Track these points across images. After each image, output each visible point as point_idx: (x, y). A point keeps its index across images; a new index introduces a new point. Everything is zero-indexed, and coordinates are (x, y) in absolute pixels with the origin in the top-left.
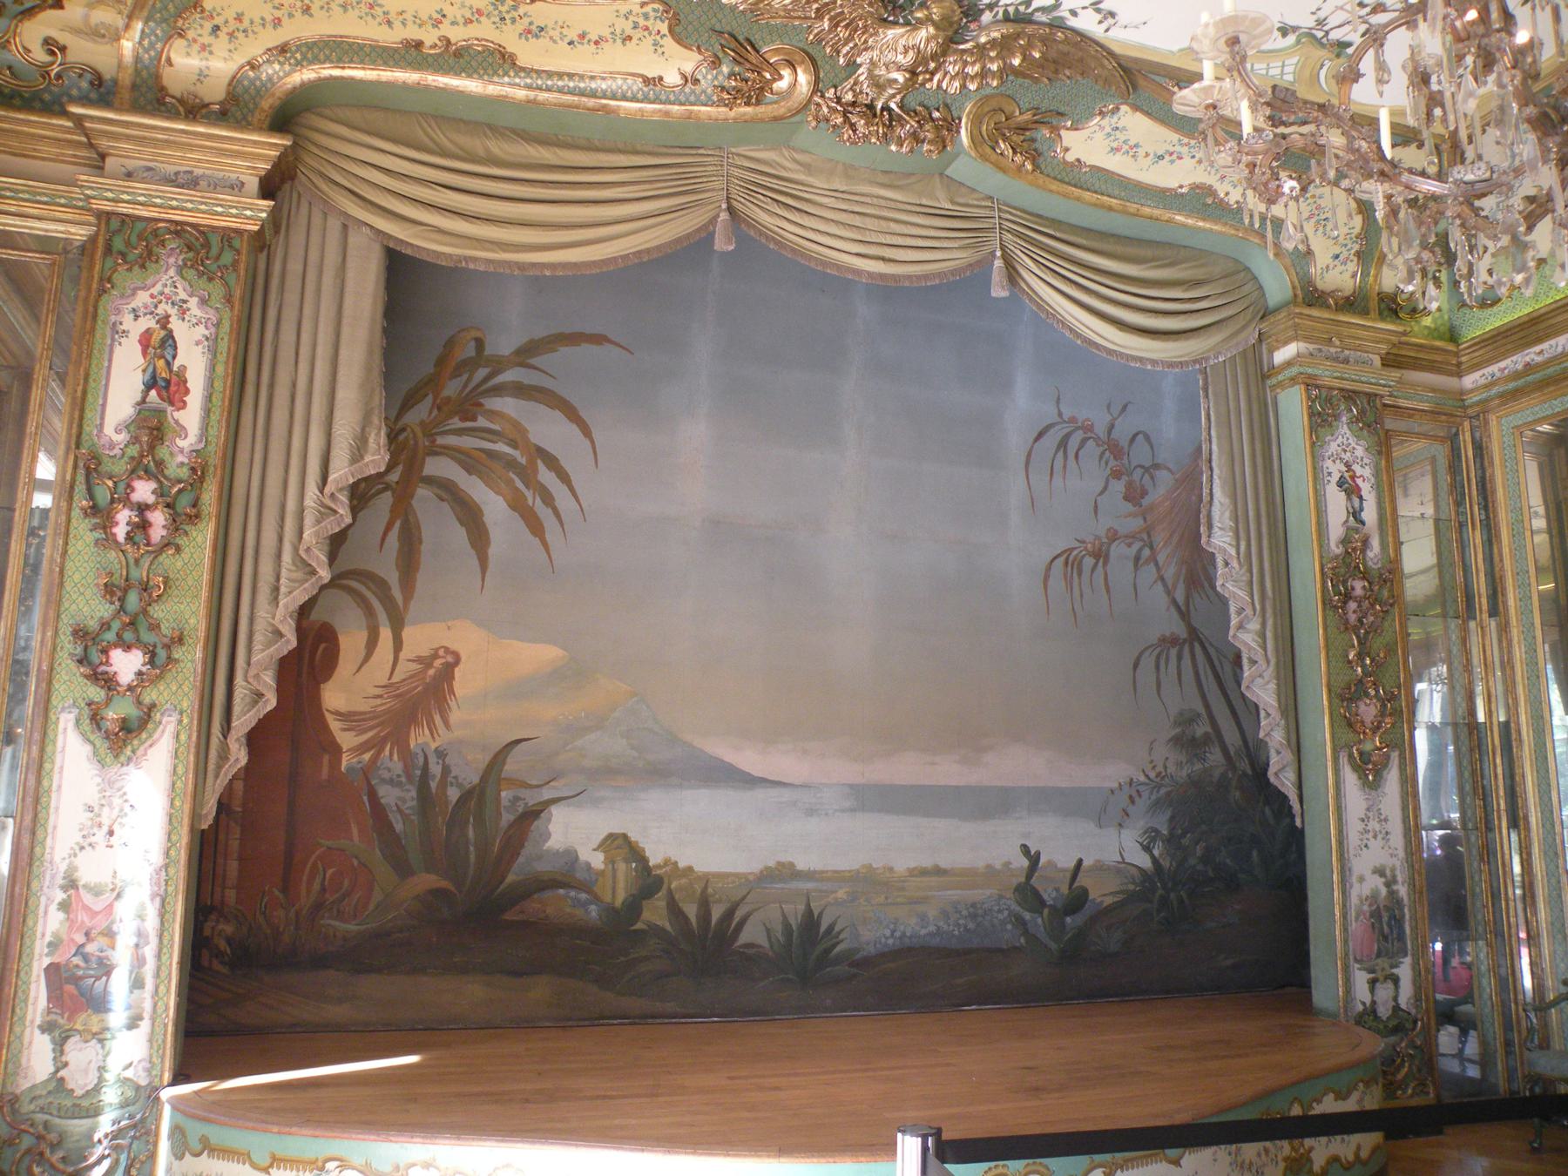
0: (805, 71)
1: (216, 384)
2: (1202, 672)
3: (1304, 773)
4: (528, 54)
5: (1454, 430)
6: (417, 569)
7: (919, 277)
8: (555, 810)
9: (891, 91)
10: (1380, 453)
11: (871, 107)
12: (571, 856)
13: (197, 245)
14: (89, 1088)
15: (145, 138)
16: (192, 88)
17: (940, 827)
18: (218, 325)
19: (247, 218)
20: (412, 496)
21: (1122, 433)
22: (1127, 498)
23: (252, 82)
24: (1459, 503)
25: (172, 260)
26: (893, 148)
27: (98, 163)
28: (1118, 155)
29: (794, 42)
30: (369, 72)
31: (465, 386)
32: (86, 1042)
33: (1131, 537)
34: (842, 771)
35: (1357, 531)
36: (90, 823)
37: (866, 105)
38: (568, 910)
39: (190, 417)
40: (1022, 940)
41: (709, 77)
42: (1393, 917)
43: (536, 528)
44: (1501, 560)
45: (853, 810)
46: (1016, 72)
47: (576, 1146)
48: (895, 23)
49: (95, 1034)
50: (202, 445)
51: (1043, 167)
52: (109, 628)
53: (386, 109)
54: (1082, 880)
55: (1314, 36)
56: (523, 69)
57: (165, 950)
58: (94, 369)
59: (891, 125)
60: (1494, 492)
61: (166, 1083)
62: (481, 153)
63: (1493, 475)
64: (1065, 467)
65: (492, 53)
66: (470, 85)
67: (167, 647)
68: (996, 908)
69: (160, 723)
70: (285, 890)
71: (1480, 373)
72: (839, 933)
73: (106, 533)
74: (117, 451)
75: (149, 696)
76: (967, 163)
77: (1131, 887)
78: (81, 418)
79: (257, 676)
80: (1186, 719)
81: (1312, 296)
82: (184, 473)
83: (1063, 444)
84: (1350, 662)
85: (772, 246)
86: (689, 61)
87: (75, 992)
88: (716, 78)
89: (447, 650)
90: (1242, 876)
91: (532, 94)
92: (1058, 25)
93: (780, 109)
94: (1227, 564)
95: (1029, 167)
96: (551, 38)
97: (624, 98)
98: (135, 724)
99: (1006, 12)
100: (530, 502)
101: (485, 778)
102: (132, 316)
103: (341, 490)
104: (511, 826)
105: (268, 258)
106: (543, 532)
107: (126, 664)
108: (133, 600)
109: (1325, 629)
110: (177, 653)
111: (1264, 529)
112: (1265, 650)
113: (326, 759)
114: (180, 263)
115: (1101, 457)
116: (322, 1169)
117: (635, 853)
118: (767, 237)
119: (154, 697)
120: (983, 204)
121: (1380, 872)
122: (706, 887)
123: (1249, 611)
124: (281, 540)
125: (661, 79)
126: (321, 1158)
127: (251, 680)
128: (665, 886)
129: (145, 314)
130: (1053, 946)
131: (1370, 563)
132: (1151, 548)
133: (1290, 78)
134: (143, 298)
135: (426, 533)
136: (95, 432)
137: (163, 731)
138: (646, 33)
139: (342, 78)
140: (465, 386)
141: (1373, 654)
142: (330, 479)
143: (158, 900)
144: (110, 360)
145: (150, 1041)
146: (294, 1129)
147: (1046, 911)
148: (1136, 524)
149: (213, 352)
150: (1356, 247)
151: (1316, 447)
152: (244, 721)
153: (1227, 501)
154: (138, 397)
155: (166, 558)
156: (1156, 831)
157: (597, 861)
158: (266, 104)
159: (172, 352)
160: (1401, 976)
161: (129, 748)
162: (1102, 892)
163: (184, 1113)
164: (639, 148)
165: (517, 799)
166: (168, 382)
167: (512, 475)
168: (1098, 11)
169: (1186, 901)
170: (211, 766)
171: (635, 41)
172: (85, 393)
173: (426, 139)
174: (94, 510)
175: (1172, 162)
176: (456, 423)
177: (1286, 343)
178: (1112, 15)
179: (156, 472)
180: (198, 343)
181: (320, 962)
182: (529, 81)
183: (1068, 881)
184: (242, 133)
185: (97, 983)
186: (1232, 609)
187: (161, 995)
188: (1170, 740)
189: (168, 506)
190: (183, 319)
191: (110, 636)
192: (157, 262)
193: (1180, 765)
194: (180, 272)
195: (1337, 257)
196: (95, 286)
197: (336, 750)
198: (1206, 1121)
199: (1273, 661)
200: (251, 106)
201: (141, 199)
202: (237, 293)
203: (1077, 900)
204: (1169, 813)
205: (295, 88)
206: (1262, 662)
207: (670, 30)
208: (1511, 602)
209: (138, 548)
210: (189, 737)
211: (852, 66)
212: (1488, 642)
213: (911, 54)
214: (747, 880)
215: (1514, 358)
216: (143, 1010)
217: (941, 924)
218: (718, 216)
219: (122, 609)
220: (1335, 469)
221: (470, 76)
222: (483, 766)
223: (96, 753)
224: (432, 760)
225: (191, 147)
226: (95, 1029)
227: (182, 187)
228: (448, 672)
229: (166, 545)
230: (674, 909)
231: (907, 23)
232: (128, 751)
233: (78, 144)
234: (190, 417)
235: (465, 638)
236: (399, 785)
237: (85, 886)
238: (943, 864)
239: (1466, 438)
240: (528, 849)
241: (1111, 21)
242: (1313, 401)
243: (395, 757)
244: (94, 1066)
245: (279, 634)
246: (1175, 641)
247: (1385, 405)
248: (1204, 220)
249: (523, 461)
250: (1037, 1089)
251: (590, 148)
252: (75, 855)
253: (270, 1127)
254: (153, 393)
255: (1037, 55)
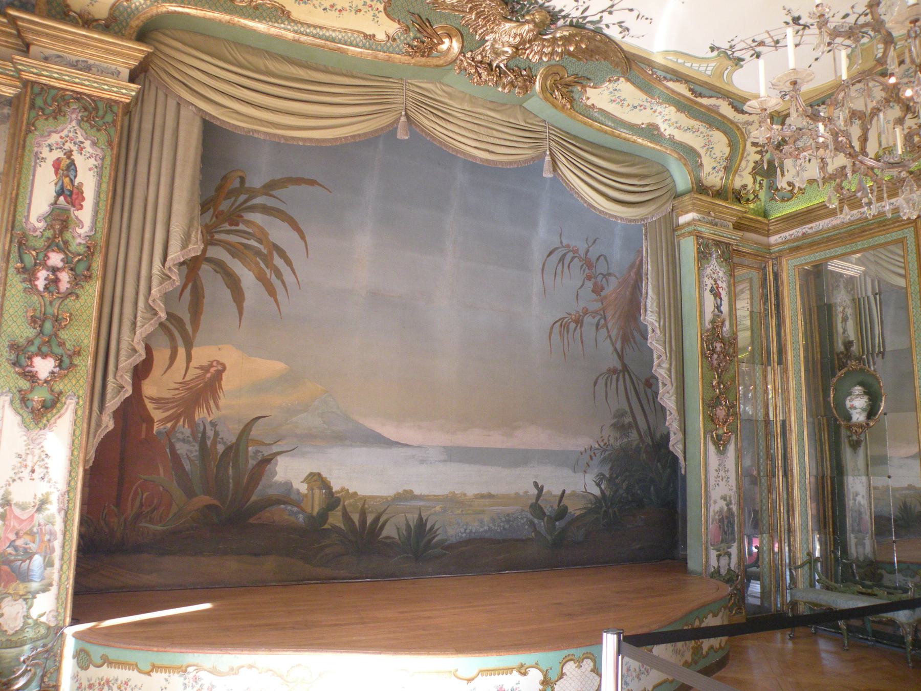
0: (457, 41)
1: (102, 196)
2: (628, 388)
3: (687, 447)
4: (298, 12)
5: (763, 265)
6: (201, 313)
7: (507, 163)
8: (280, 459)
9: (503, 58)
10: (731, 275)
11: (490, 65)
12: (288, 486)
13: (90, 107)
14: (17, 629)
15: (58, 37)
16: (87, 8)
17: (492, 471)
18: (103, 159)
19: (123, 94)
20: (199, 269)
21: (592, 255)
22: (593, 291)
23: (125, 9)
24: (765, 303)
25: (74, 116)
26: (500, 89)
27: (26, 49)
28: (614, 103)
29: (453, 24)
30: (199, 12)
31: (233, 204)
32: (16, 600)
33: (595, 313)
34: (441, 439)
35: (718, 316)
36: (19, 465)
37: (488, 64)
38: (287, 517)
39: (85, 215)
40: (533, 534)
41: (402, 38)
42: (729, 522)
43: (272, 292)
44: (785, 335)
45: (445, 461)
46: (570, 54)
47: (341, 652)
48: (511, 20)
49: (21, 596)
50: (93, 233)
51: (575, 107)
52: (33, 344)
53: (202, 34)
54: (565, 502)
55: (727, 53)
56: (294, 21)
57: (67, 543)
58: (23, 181)
59: (500, 76)
60: (783, 299)
61: (67, 624)
62: (263, 68)
63: (783, 290)
64: (562, 272)
65: (276, 9)
66: (261, 27)
67: (70, 357)
68: (520, 517)
69: (65, 403)
70: (118, 504)
71: (779, 236)
72: (437, 530)
73: (31, 284)
74: (38, 233)
75: (58, 386)
76: (536, 103)
77: (590, 506)
78: (15, 211)
79: (122, 376)
80: (620, 414)
81: (701, 188)
82: (82, 249)
83: (562, 259)
84: (713, 386)
85: (428, 139)
86: (393, 28)
87: (9, 570)
88: (406, 39)
89: (218, 362)
90: (645, 500)
91: (297, 36)
92: (598, 32)
93: (434, 61)
94: (653, 331)
95: (569, 106)
96: (314, 5)
97: (351, 45)
98: (49, 404)
99: (572, 21)
100: (268, 276)
101: (239, 439)
102: (48, 149)
103: (174, 265)
104: (254, 468)
105: (130, 121)
106: (276, 295)
107: (44, 367)
108: (48, 326)
109: (702, 368)
110: (77, 361)
111: (672, 313)
112: (670, 377)
113: (144, 426)
114: (79, 118)
115: (581, 268)
116: (185, 671)
117: (325, 485)
118: (426, 133)
119: (61, 388)
120: (541, 124)
121: (724, 498)
122: (364, 504)
123: (664, 357)
124: (137, 293)
125: (374, 36)
126: (185, 664)
127: (117, 378)
128: (342, 503)
129: (57, 148)
130: (549, 537)
131: (724, 334)
132: (605, 320)
133: (709, 73)
134: (55, 138)
135: (207, 292)
136: (24, 220)
137: (67, 409)
138: (370, 9)
139: (182, 13)
140: (233, 204)
141: (724, 383)
142: (168, 258)
143: (63, 513)
144: (34, 176)
145: (57, 599)
146: (168, 649)
147: (546, 519)
148: (597, 306)
149: (100, 176)
150: (725, 164)
151: (700, 269)
152: (113, 403)
153: (655, 297)
154: (52, 200)
155: (70, 301)
156: (604, 475)
157: (303, 488)
158: (135, 23)
159: (74, 174)
160: (732, 553)
161: (45, 418)
162: (575, 508)
163: (83, 640)
164: (354, 73)
165: (257, 452)
166: (71, 192)
167: (258, 259)
168: (621, 27)
169: (617, 514)
170: (92, 430)
171: (362, 12)
172: (17, 195)
173: (228, 54)
174: (24, 270)
175: (640, 110)
176: (227, 226)
177: (687, 212)
178: (628, 30)
179: (64, 248)
180: (90, 169)
181: (139, 549)
182: (296, 28)
183: (557, 501)
184: (118, 39)
185: (23, 564)
186: (655, 356)
187: (64, 570)
188: (612, 425)
189: (72, 269)
190: (81, 154)
191: (34, 349)
192: (64, 116)
193: (616, 439)
194: (79, 124)
195: (714, 168)
196: (24, 128)
197: (150, 421)
198: (660, 631)
199: (675, 385)
200: (124, 24)
201: (56, 75)
202: (116, 141)
203: (562, 512)
204: (610, 465)
205: (152, 16)
206: (669, 385)
207: (385, 9)
208: (789, 358)
209: (52, 295)
210: (83, 413)
211: (483, 41)
212: (776, 378)
213: (518, 39)
214: (387, 500)
215: (797, 230)
216: (53, 579)
217: (491, 525)
218: (399, 118)
219: (41, 332)
220: (709, 283)
221: (260, 21)
222: (238, 432)
223: (23, 421)
224: (208, 428)
225: (88, 46)
226: (21, 593)
227: (80, 70)
228: (219, 375)
229: (70, 294)
230: (346, 516)
231: (518, 21)
232: (44, 421)
233: (11, 35)
234: (85, 215)
235: (228, 355)
236: (189, 442)
237: (16, 504)
238: (493, 491)
239: (770, 269)
240: (264, 481)
241: (626, 33)
242: (700, 245)
243: (186, 426)
244: (21, 615)
245: (134, 351)
246: (614, 371)
247: (734, 250)
248: (651, 143)
249: (265, 251)
250: (570, 615)
251: (326, 71)
252: (9, 485)
253: (151, 648)
254: (62, 198)
255: (584, 46)
